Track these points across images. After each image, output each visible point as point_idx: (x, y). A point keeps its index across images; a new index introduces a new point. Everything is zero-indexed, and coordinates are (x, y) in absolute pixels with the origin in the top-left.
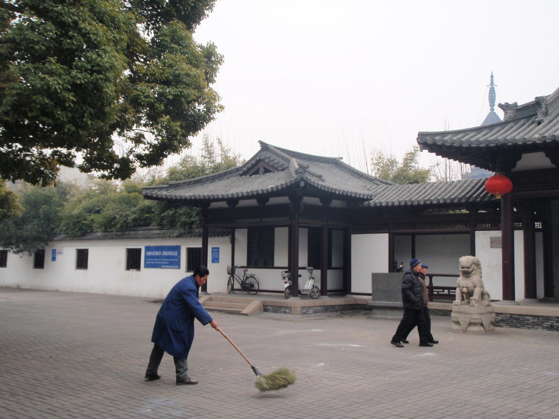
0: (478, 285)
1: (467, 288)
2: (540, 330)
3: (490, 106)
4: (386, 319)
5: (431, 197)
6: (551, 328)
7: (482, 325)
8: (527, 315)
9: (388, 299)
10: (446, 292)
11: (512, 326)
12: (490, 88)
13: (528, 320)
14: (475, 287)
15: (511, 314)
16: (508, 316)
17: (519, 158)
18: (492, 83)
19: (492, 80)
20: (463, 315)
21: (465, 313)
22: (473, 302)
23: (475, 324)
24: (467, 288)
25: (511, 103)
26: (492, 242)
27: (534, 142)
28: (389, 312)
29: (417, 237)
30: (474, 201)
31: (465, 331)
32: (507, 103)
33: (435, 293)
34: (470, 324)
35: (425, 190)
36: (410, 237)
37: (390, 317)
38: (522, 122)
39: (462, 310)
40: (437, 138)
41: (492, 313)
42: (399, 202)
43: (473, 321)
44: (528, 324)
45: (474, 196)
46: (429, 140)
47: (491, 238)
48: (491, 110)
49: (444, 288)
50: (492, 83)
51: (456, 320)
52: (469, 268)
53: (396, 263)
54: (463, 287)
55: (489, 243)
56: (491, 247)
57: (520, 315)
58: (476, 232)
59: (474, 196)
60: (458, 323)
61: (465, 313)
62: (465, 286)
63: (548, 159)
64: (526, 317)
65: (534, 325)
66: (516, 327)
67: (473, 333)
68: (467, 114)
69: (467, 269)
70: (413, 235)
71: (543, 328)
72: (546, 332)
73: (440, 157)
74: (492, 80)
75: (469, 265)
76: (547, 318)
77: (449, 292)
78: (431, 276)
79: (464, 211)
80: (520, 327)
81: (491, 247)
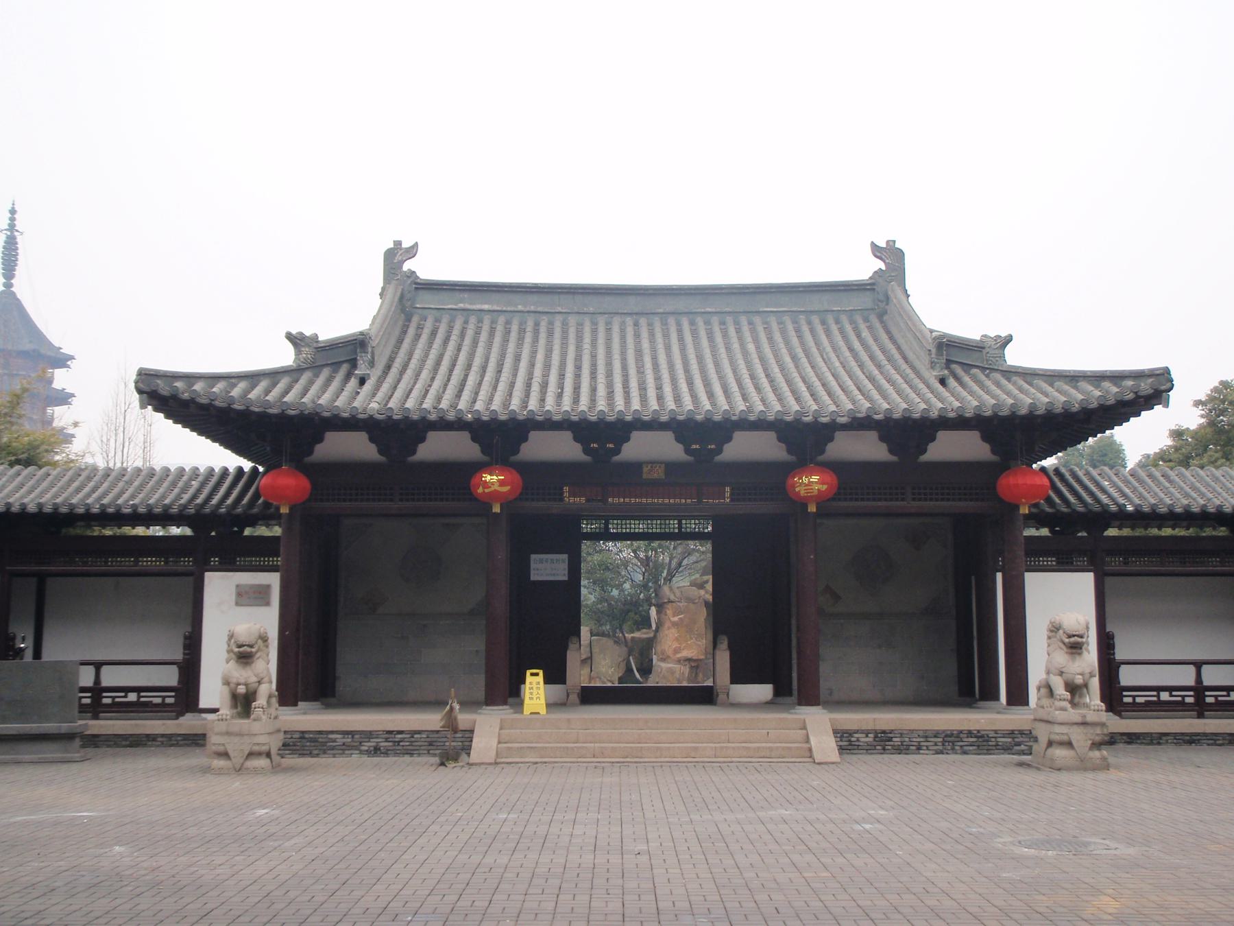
0: (266, 679)
1: (246, 685)
2: (355, 757)
3: (5, 276)
4: (18, 763)
5: (88, 495)
6: (376, 751)
7: (268, 755)
8: (332, 732)
9: (23, 717)
10: (132, 697)
11: (303, 755)
12: (8, 237)
13: (334, 741)
14: (259, 683)
15: (303, 732)
16: (297, 736)
17: (320, 439)
18: (12, 227)
19: (12, 219)
20: (236, 739)
21: (240, 735)
22: (257, 712)
23: (259, 754)
24: (246, 685)
25: (308, 333)
26: (239, 594)
27: (371, 417)
28: (24, 747)
29: (52, 585)
30: (228, 513)
31: (239, 770)
32: (301, 334)
33: (105, 701)
34: (251, 755)
35: (92, 484)
36: (33, 581)
37: (27, 757)
38: (326, 372)
39: (236, 729)
40: (198, 387)
41: (279, 731)
42: (40, 506)
43: (256, 748)
44: (333, 748)
45: (229, 501)
46: (164, 388)
47: (237, 586)
48: (5, 285)
49: (127, 690)
50: (12, 227)
51: (221, 749)
52: (251, 646)
53: (14, 638)
54: (239, 684)
55: (234, 597)
56: (237, 604)
57: (320, 732)
58: (207, 574)
59: (229, 501)
60: (225, 755)
61: (240, 735)
62: (242, 681)
63: (373, 446)
64: (331, 736)
65: (345, 749)
66: (311, 755)
67: (256, 771)
68: (243, 344)
69: (248, 649)
70: (42, 578)
71: (361, 752)
72: (365, 759)
73: (161, 415)
74: (12, 219)
75: (251, 640)
76: (369, 735)
77: (139, 697)
78: (98, 666)
79: (175, 531)
80: (317, 755)
81: (237, 604)
